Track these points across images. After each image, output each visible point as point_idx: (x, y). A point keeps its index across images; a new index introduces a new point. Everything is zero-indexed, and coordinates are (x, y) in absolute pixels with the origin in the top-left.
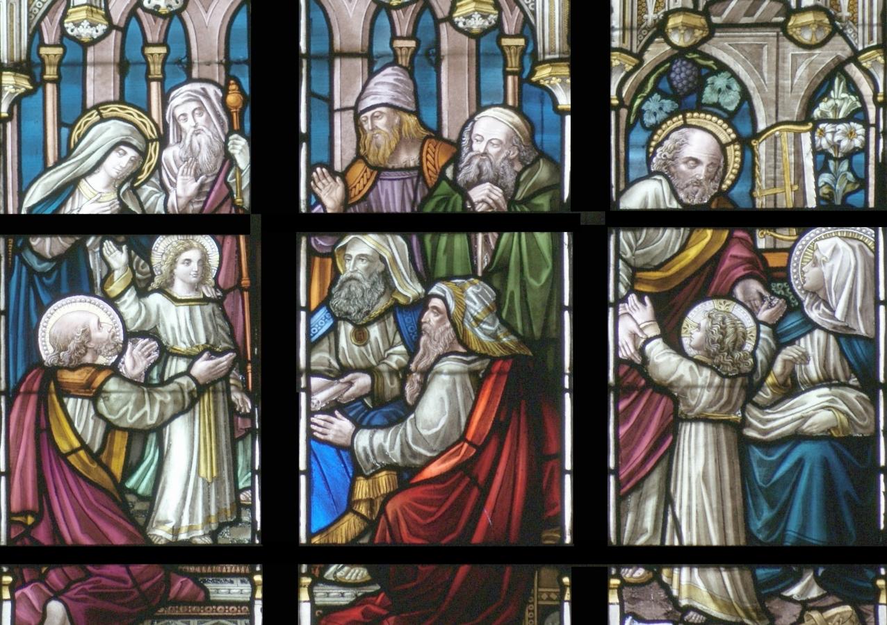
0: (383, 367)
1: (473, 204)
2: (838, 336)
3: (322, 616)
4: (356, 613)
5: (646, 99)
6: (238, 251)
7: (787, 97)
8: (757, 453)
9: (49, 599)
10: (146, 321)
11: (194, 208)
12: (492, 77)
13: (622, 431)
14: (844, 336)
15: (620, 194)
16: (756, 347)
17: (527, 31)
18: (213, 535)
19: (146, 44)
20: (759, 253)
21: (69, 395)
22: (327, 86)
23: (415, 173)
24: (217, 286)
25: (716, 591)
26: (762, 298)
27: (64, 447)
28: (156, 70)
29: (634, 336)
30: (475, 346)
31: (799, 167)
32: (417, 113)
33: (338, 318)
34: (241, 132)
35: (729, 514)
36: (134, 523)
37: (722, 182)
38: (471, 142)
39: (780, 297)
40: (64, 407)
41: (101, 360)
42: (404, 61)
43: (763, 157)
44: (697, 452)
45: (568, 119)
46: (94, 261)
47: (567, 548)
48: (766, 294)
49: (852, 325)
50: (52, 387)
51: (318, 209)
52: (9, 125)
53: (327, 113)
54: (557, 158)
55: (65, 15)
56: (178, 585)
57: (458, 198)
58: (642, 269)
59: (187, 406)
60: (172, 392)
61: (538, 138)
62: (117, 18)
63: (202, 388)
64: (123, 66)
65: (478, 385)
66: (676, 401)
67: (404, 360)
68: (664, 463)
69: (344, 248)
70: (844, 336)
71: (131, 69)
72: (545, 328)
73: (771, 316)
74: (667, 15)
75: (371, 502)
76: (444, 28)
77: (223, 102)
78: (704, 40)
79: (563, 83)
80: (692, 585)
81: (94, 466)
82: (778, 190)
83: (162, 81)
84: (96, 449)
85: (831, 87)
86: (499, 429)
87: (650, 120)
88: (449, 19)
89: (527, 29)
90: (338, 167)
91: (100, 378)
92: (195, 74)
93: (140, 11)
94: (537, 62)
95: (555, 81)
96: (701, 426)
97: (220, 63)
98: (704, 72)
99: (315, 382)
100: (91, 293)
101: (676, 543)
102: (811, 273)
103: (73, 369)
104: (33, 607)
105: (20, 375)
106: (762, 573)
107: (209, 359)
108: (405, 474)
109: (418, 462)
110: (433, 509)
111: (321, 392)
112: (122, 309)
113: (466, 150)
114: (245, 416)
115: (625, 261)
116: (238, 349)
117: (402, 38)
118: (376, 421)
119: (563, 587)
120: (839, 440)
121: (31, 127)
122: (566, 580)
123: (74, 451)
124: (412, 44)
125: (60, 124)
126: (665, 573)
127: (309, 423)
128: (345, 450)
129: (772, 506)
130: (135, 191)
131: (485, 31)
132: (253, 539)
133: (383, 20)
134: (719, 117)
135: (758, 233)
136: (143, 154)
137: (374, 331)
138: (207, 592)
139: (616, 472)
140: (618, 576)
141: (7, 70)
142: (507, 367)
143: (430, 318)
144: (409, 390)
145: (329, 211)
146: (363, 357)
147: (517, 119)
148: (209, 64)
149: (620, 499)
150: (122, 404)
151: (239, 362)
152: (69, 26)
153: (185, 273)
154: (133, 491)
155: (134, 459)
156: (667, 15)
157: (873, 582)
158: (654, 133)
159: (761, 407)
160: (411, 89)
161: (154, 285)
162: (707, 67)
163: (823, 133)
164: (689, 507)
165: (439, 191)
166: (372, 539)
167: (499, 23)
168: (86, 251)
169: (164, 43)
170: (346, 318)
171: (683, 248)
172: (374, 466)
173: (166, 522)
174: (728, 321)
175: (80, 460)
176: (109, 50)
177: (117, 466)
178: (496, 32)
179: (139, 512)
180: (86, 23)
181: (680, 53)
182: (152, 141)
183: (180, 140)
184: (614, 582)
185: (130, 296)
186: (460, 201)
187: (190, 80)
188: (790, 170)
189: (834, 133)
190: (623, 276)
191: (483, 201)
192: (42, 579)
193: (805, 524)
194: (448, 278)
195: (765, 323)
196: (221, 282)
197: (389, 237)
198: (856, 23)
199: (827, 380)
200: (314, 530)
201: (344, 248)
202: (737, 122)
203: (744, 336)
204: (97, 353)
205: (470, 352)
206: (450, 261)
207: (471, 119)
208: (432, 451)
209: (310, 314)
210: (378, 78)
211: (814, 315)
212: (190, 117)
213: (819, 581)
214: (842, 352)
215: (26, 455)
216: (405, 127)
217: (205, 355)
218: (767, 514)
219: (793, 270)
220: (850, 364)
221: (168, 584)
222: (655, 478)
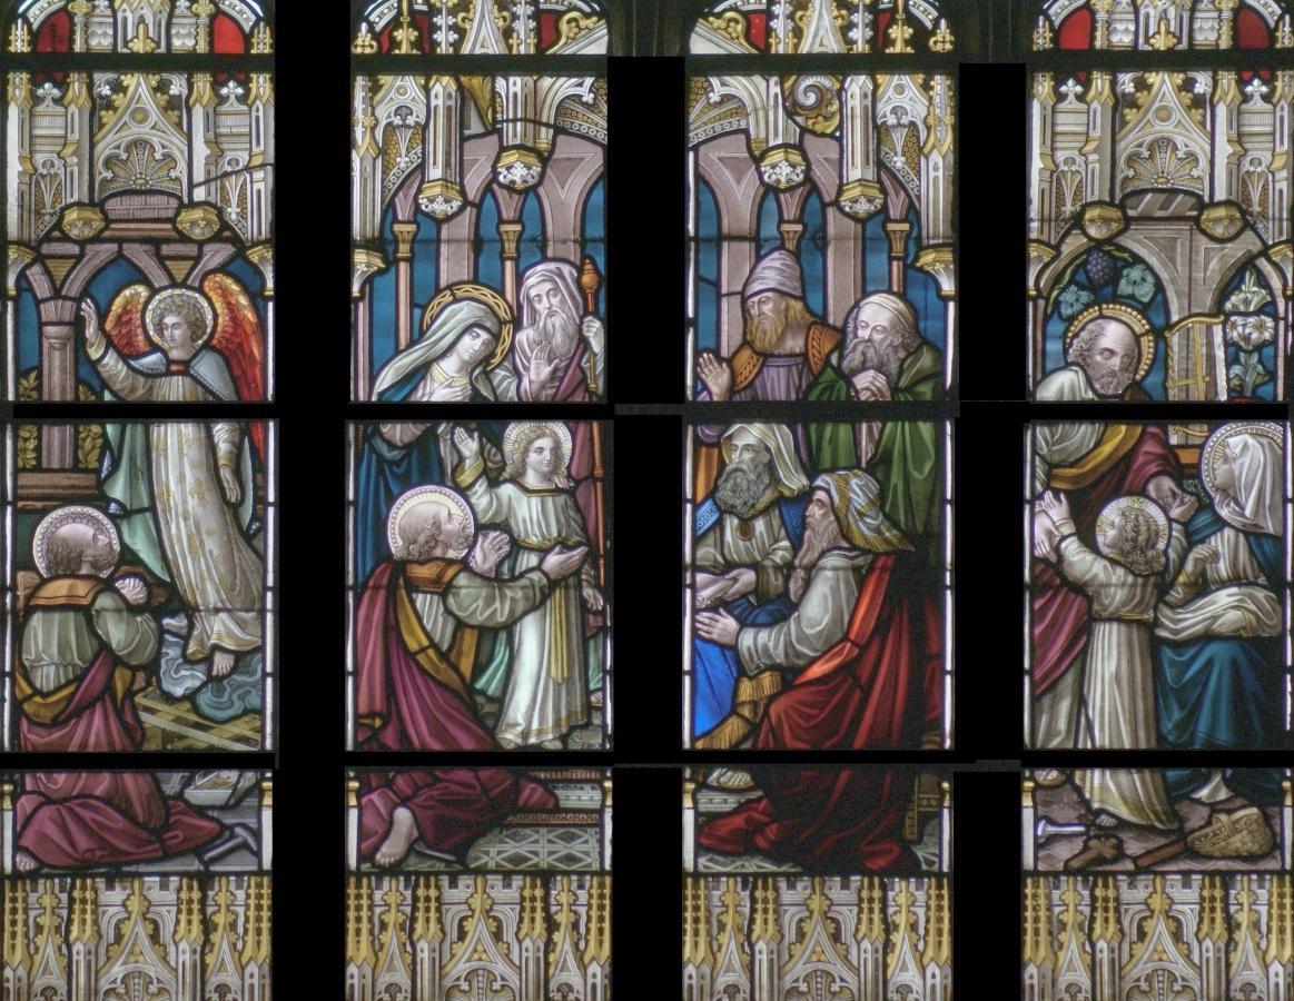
0: (767, 563)
1: (857, 392)
2: (1246, 534)
3: (706, 824)
4: (739, 821)
5: (1063, 290)
6: (592, 439)
7: (1199, 289)
8: (1168, 653)
9: (396, 806)
10: (497, 512)
11: (546, 395)
12: (878, 262)
13: (1038, 631)
14: (1252, 534)
15: (1037, 384)
16: (1168, 545)
17: (912, 217)
18: (564, 738)
19: (501, 221)
20: (1171, 449)
21: (418, 591)
22: (714, 270)
23: (800, 360)
24: (569, 476)
25: (1127, 793)
26: (1174, 495)
27: (413, 646)
28: (510, 247)
29: (1050, 534)
30: (859, 541)
31: (1211, 358)
32: (803, 298)
33: (724, 511)
34: (596, 314)
35: (1141, 716)
36: (482, 725)
37: (1136, 372)
38: (856, 328)
39: (1192, 494)
40: (412, 602)
41: (451, 554)
42: (791, 245)
43: (1176, 349)
44: (1110, 653)
45: (952, 306)
46: (444, 449)
47: (947, 752)
48: (1178, 492)
49: (1261, 523)
50: (401, 581)
51: (703, 397)
52: (361, 305)
53: (714, 298)
54: (940, 345)
55: (419, 190)
56: (527, 792)
57: (842, 384)
58: (1058, 466)
59: (536, 605)
60: (523, 588)
61: (922, 325)
62: (472, 194)
63: (553, 584)
64: (477, 244)
65: (861, 584)
66: (1090, 600)
67: (788, 556)
68: (1078, 664)
69: (731, 437)
70: (1252, 534)
71: (486, 247)
72: (926, 525)
73: (1183, 514)
74: (1085, 207)
75: (754, 704)
76: (831, 212)
77: (578, 282)
78: (1120, 233)
79: (946, 269)
80: (1104, 787)
81: (443, 666)
82: (1190, 381)
83: (516, 260)
84: (445, 647)
85: (1242, 280)
86: (881, 628)
87: (1066, 311)
88: (836, 203)
89: (912, 213)
90: (725, 353)
91: (450, 572)
92: (550, 253)
93: (495, 186)
94: (921, 248)
95: (939, 266)
96: (1115, 626)
97: (575, 241)
98: (1120, 264)
99: (701, 577)
100: (442, 483)
101: (1089, 746)
102: (1221, 470)
103: (421, 563)
104: (380, 814)
105: (368, 568)
106: (1172, 774)
107: (561, 553)
108: (789, 674)
109: (801, 662)
110: (813, 712)
111: (706, 588)
112: (473, 500)
113: (851, 336)
114: (597, 613)
115: (1042, 457)
116: (590, 543)
117: (789, 222)
118: (760, 620)
119: (942, 793)
120: (1247, 639)
121: (383, 308)
122: (946, 785)
123: (423, 650)
124: (799, 228)
125: (413, 305)
126: (1078, 774)
127: (694, 621)
128: (730, 649)
129: (1182, 708)
130: (487, 375)
131: (871, 216)
132: (603, 744)
133: (771, 204)
134: (1133, 308)
135: (1171, 429)
136: (496, 337)
137: (760, 526)
138: (557, 799)
139: (1031, 673)
140: (1032, 778)
141: (360, 247)
142: (890, 563)
143: (815, 511)
144: (794, 587)
145: (715, 399)
146: (749, 552)
147: (901, 306)
148: (564, 242)
149: (1035, 699)
150: (472, 600)
151: (591, 557)
152: (423, 201)
153: (538, 459)
154: (483, 693)
155: (483, 658)
156: (1085, 207)
157: (1280, 784)
158: (1071, 324)
159: (1172, 607)
160: (798, 274)
161: (506, 475)
162: (1124, 260)
163: (1234, 326)
164: (1102, 708)
165: (822, 379)
166: (755, 744)
167: (885, 208)
168: (437, 437)
169: (519, 221)
170: (731, 511)
171: (1098, 444)
172: (758, 667)
173: (517, 725)
174: (1141, 519)
175: (429, 660)
176: (463, 227)
177: (466, 666)
178: (882, 217)
179: (488, 714)
180: (440, 199)
181: (1097, 245)
182: (506, 322)
183: (534, 322)
184: (1028, 785)
185: (481, 487)
186: (844, 389)
187: (545, 259)
188: (1203, 363)
189: (1244, 326)
190: (1040, 472)
191: (867, 389)
192: (390, 784)
193: (1214, 726)
194: (832, 470)
195: (1177, 521)
196: (573, 472)
197: (775, 427)
198: (1265, 218)
199: (1236, 580)
200: (697, 733)
201: (731, 437)
202: (1151, 313)
203: (1157, 535)
204: (447, 546)
205: (854, 547)
206: (835, 451)
207: (857, 305)
208: (815, 650)
209: (696, 507)
210: (765, 263)
211: (1224, 513)
212: (545, 299)
213: (1227, 782)
214: (1251, 552)
215: (373, 658)
216: (792, 312)
217: (557, 549)
218: (1177, 715)
219: (1204, 467)
220: (1259, 564)
221: (518, 791)
222: (1069, 679)
